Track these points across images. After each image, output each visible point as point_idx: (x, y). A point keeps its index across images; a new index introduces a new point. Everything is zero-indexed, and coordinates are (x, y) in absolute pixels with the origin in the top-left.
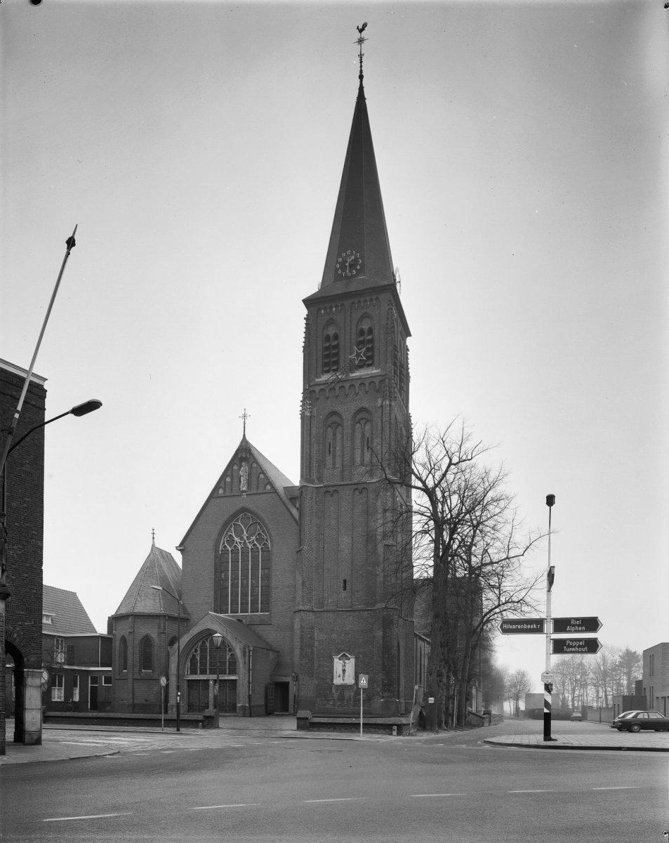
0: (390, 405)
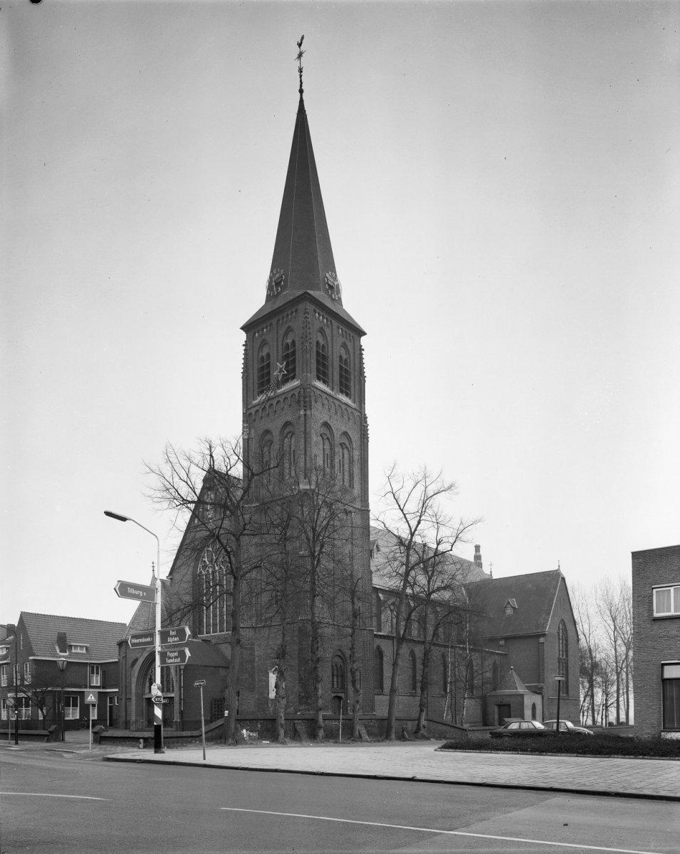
0: (305, 415)
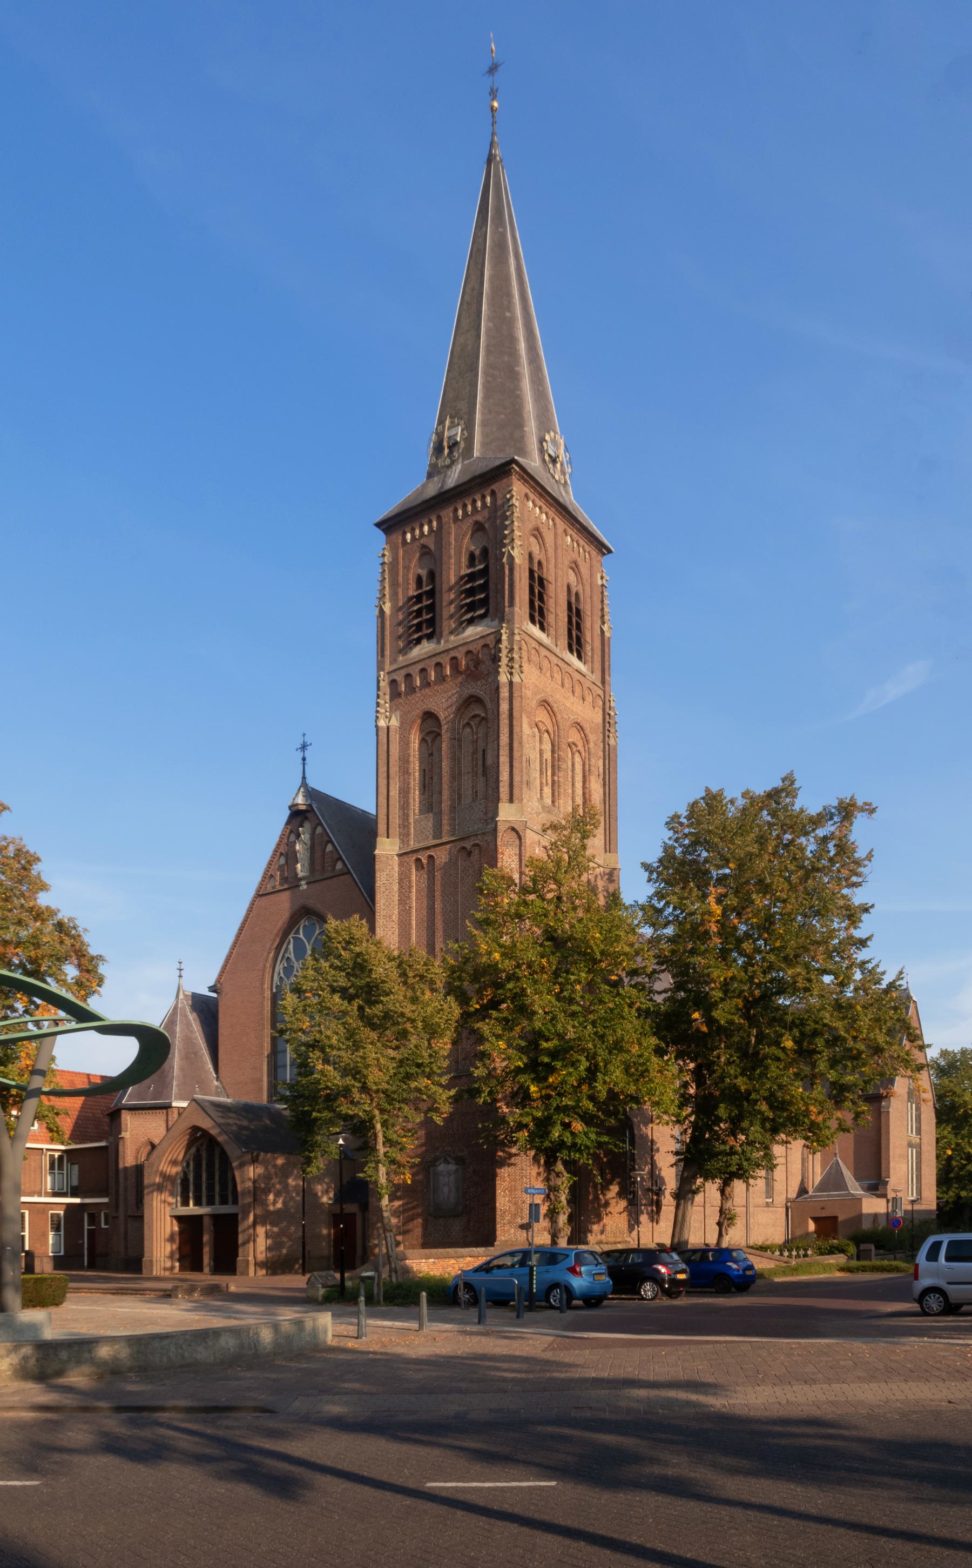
0: (511, 683)
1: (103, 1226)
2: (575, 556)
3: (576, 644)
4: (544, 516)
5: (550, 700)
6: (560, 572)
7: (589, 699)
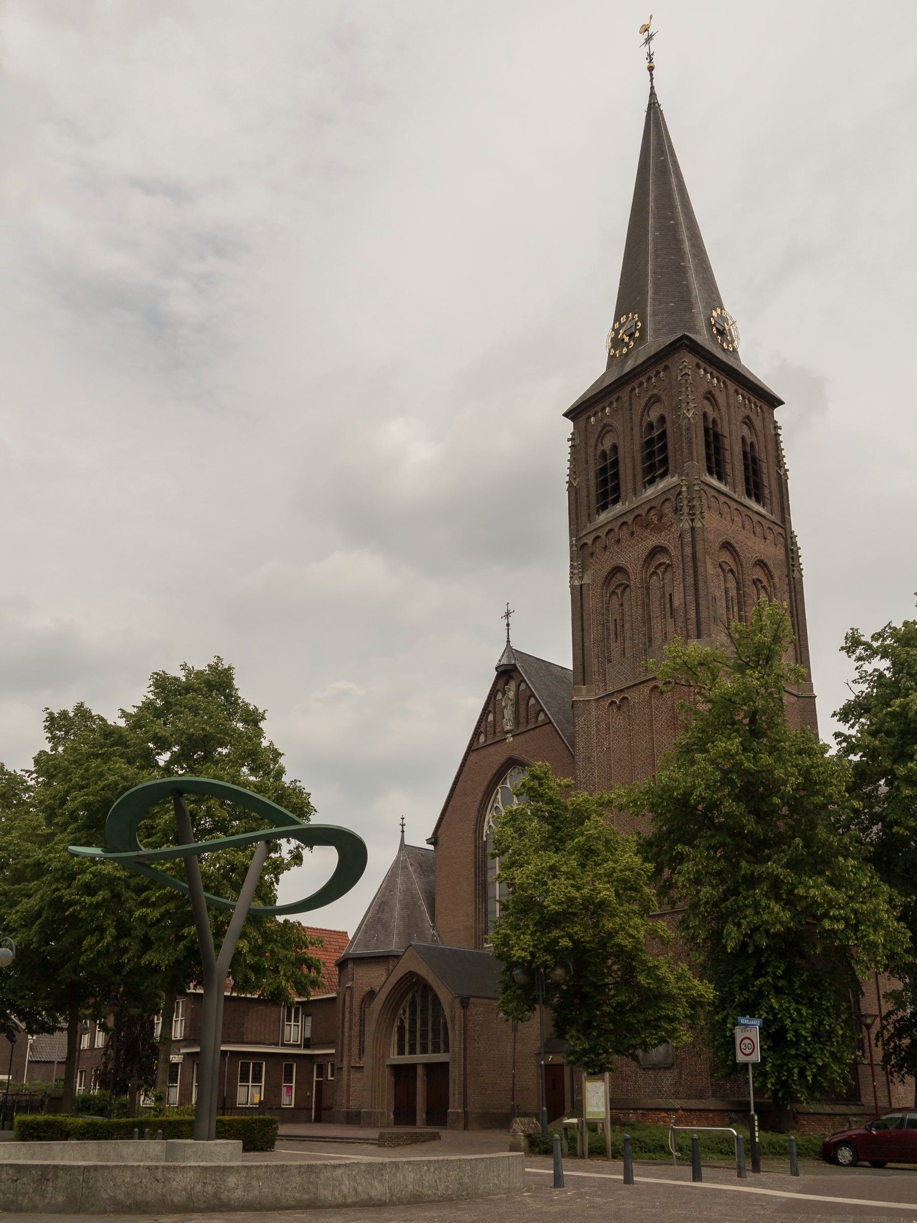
0: (693, 529)
1: (330, 1078)
2: (747, 412)
3: (755, 489)
4: (715, 381)
5: (732, 542)
6: (734, 427)
7: (770, 537)
